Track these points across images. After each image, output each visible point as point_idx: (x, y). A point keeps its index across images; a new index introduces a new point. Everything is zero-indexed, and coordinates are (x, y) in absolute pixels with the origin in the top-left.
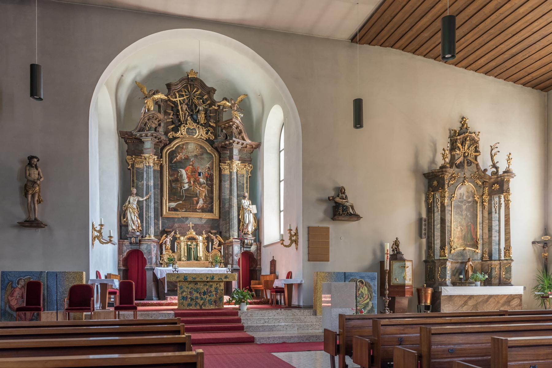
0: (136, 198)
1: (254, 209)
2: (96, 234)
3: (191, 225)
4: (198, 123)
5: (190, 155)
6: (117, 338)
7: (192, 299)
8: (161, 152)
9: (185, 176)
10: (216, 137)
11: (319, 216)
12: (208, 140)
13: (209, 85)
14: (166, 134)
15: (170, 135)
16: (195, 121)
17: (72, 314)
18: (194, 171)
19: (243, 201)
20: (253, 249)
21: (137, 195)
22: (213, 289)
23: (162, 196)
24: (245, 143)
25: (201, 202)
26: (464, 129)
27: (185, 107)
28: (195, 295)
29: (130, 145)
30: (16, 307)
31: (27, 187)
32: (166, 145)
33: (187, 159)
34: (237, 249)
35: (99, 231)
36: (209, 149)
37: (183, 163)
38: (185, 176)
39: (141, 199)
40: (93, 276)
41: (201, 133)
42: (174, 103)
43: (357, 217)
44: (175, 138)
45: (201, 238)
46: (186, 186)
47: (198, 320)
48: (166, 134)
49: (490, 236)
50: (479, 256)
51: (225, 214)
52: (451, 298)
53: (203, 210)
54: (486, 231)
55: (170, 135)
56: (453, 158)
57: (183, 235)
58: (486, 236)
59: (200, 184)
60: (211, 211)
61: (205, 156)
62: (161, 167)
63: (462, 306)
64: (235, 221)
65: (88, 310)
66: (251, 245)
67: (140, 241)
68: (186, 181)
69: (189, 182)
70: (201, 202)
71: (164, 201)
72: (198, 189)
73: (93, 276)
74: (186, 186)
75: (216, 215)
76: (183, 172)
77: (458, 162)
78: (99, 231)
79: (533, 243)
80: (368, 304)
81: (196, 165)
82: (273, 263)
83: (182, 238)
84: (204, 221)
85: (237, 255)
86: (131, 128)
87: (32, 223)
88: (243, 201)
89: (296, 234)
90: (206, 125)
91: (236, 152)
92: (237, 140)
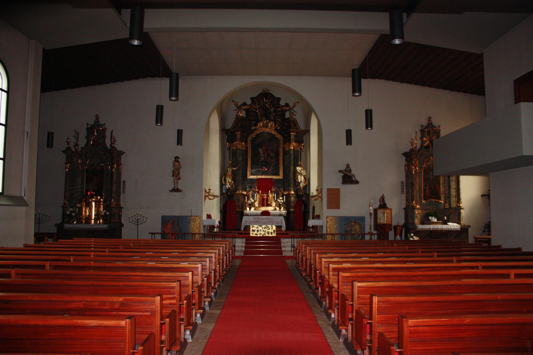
6: (263, 177)
7: (258, 231)
9: (261, 152)
11: (334, 181)
16: (267, 118)
20: (304, 198)
26: (430, 125)
31: (176, 174)
35: (208, 193)
38: (261, 152)
42: (256, 109)
43: (357, 182)
47: (422, 263)
49: (450, 192)
50: (442, 205)
54: (447, 188)
60: (278, 174)
62: (247, 148)
64: (292, 181)
69: (264, 157)
73: (205, 217)
74: (262, 159)
76: (261, 150)
79: (482, 196)
82: (314, 208)
85: (293, 203)
87: (176, 190)
90: (274, 121)
92: (292, 130)
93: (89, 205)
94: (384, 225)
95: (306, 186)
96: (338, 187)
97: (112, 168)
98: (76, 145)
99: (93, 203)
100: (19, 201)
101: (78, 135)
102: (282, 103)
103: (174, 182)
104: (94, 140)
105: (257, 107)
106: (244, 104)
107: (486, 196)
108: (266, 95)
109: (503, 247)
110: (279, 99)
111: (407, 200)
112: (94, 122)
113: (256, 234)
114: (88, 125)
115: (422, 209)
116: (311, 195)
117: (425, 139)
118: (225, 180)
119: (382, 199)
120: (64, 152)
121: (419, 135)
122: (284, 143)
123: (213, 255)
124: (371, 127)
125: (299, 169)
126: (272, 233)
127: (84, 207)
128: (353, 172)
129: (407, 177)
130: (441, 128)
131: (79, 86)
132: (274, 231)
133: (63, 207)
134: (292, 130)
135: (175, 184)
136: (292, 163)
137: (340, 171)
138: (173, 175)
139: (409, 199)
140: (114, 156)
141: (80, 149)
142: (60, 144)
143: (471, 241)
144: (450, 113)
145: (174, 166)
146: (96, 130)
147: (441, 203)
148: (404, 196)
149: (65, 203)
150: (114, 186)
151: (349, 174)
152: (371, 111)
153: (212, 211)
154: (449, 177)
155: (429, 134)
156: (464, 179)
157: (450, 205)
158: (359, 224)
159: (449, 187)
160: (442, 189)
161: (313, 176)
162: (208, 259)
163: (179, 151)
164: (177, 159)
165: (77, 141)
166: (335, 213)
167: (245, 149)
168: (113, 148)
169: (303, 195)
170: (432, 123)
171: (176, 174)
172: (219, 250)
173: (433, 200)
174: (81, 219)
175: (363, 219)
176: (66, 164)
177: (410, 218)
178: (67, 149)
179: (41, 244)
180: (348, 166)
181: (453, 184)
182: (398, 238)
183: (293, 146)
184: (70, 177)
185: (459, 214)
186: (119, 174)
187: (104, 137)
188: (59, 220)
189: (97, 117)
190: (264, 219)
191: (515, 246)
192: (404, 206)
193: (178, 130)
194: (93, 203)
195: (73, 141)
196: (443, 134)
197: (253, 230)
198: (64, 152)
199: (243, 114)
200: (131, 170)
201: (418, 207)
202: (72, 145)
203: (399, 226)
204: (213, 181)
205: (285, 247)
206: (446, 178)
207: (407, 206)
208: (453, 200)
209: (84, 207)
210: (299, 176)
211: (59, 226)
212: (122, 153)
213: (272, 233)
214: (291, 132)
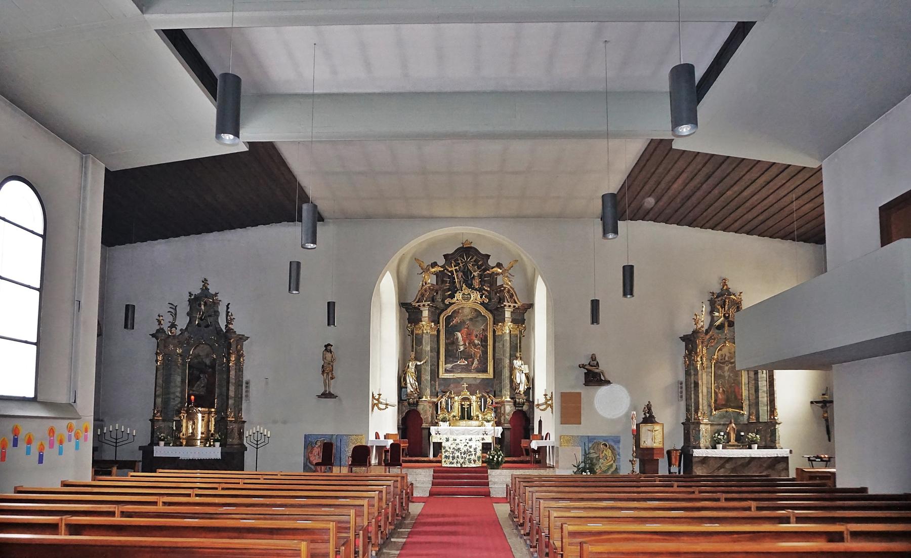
0: (414, 363)
1: (525, 369)
2: (375, 402)
3: (465, 385)
4: (473, 289)
5: (465, 318)
8: (439, 319)
10: (490, 300)
11: (575, 382)
12: (482, 304)
13: (483, 252)
14: (443, 301)
15: (447, 302)
16: (470, 286)
17: (354, 469)
18: (469, 334)
19: (515, 362)
20: (525, 408)
21: (416, 359)
22: (472, 450)
23: (438, 358)
24: (517, 306)
25: (476, 362)
27: (460, 274)
28: (458, 454)
29: (409, 313)
30: (314, 462)
32: (443, 311)
33: (463, 322)
34: (509, 409)
35: (378, 400)
36: (483, 311)
37: (457, 328)
39: (419, 363)
40: (372, 437)
41: (475, 296)
42: (451, 272)
44: (451, 304)
45: (474, 398)
46: (462, 348)
48: (443, 301)
49: (757, 397)
50: (746, 417)
51: (497, 373)
52: (705, 460)
53: (478, 371)
54: (752, 391)
55: (447, 302)
56: (713, 320)
57: (458, 394)
58: (753, 397)
59: (475, 346)
60: (485, 371)
61: (479, 319)
62: (438, 331)
63: (719, 468)
64: (507, 382)
65: (365, 465)
66: (523, 404)
67: (417, 402)
68: (462, 343)
69: (465, 344)
70: (476, 362)
71: (441, 363)
72: (473, 350)
73: (372, 437)
74: (462, 348)
75: (490, 374)
76: (459, 334)
77: (717, 323)
78: (378, 400)
79: (812, 403)
80: (611, 466)
81: (471, 327)
82: (540, 422)
83: (456, 398)
84: (478, 381)
86: (411, 299)
87: (327, 395)
88: (515, 362)
89: (551, 398)
90: (480, 290)
91: (508, 314)
92: (507, 304)
93: (191, 417)
94: (651, 450)
95: (529, 389)
96: (578, 391)
97: (229, 361)
98: (173, 325)
99: (200, 415)
100: (66, 410)
101: (175, 310)
102: (492, 262)
103: (325, 381)
104: (201, 319)
105: (454, 269)
106: (434, 265)
107: (823, 405)
108: (467, 251)
109: (871, 492)
110: (488, 256)
111: (688, 410)
112: (200, 291)
113: (451, 463)
114: (190, 294)
115: (711, 425)
116: (536, 403)
117: (717, 314)
118: (405, 379)
119: (649, 408)
120: (153, 335)
121: (706, 308)
122: (495, 323)
123: (365, 502)
124: (632, 294)
125: (517, 363)
126: (475, 461)
127: (184, 421)
128: (601, 368)
129: (688, 373)
130: (743, 296)
131: (177, 235)
132: (479, 458)
133: (152, 421)
134: (507, 304)
135: (325, 386)
136: (508, 355)
137: (583, 366)
138: (323, 372)
139: (692, 408)
140: (229, 342)
141: (178, 332)
142: (145, 324)
143: (792, 474)
144: (757, 270)
145: (324, 358)
146: (203, 303)
147: (743, 414)
148: (683, 404)
149: (154, 415)
150: (232, 388)
151: (597, 371)
152: (632, 267)
153: (383, 425)
154: (756, 373)
155: (723, 306)
156: (780, 375)
157: (758, 418)
158: (612, 449)
159: (757, 390)
160: (745, 393)
161: (540, 372)
162: (352, 512)
163: (331, 335)
164: (328, 347)
165: (175, 319)
166: (573, 430)
167: (436, 333)
168: (229, 330)
169: (523, 404)
170: (728, 289)
171: (327, 370)
172: (381, 492)
173: (730, 410)
174: (180, 438)
175: (617, 440)
176: (157, 354)
177: (692, 438)
178: (158, 331)
179: (105, 480)
180: (593, 358)
181: (763, 385)
182: (674, 469)
183: (508, 327)
184: (165, 372)
185: (773, 433)
186: (240, 369)
187: (217, 313)
188: (146, 441)
189: (205, 281)
190: (463, 437)
191: (857, 485)
192: (683, 420)
193: (329, 303)
194: (200, 415)
195: (167, 320)
196: (745, 305)
197: (446, 457)
198: (153, 335)
199: (431, 280)
200: (256, 365)
201: (705, 421)
202: (165, 326)
203: (677, 450)
204: (384, 378)
205: (495, 483)
206: (752, 374)
207: (688, 419)
208: (764, 410)
209: (184, 421)
210: (518, 374)
211: (147, 451)
212: (242, 339)
213: (475, 461)
214: (503, 303)
